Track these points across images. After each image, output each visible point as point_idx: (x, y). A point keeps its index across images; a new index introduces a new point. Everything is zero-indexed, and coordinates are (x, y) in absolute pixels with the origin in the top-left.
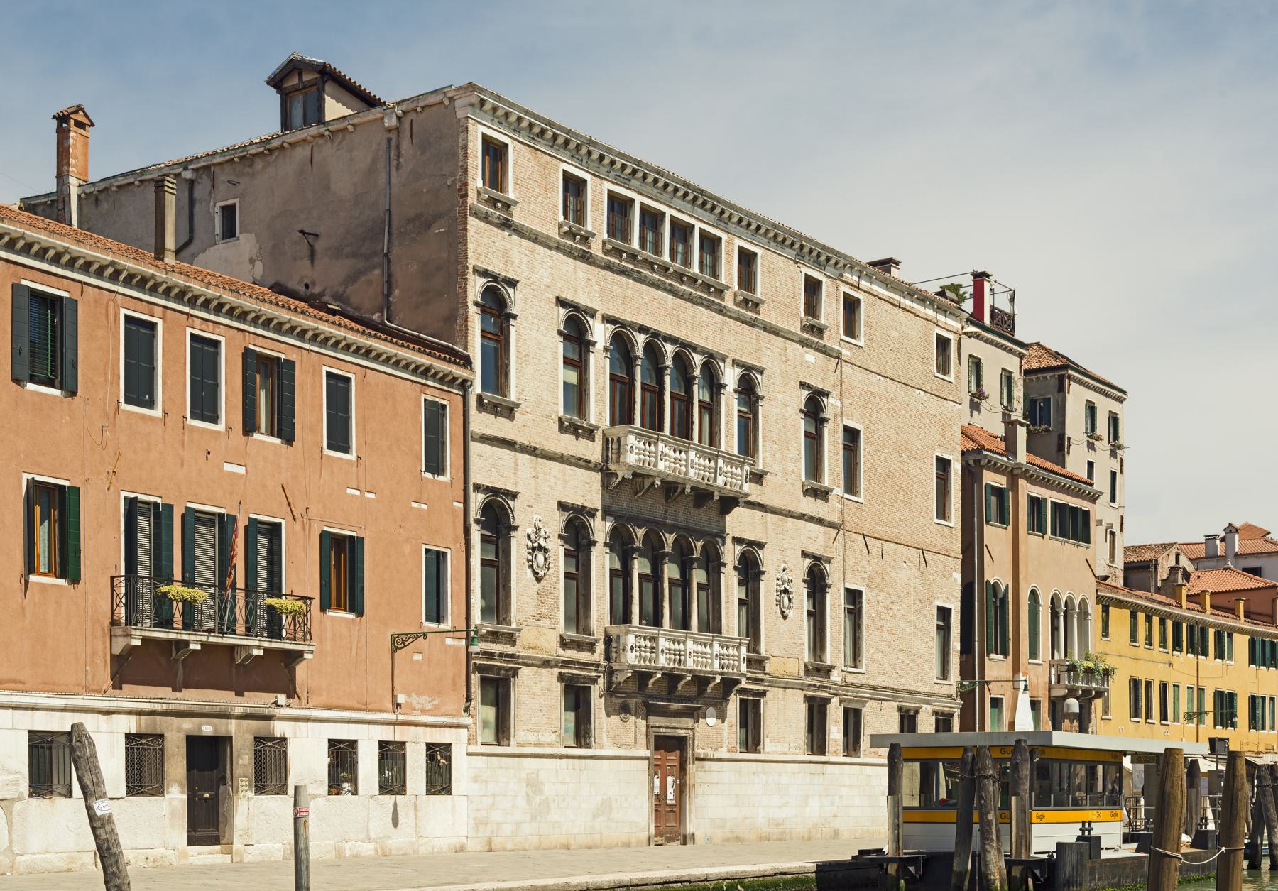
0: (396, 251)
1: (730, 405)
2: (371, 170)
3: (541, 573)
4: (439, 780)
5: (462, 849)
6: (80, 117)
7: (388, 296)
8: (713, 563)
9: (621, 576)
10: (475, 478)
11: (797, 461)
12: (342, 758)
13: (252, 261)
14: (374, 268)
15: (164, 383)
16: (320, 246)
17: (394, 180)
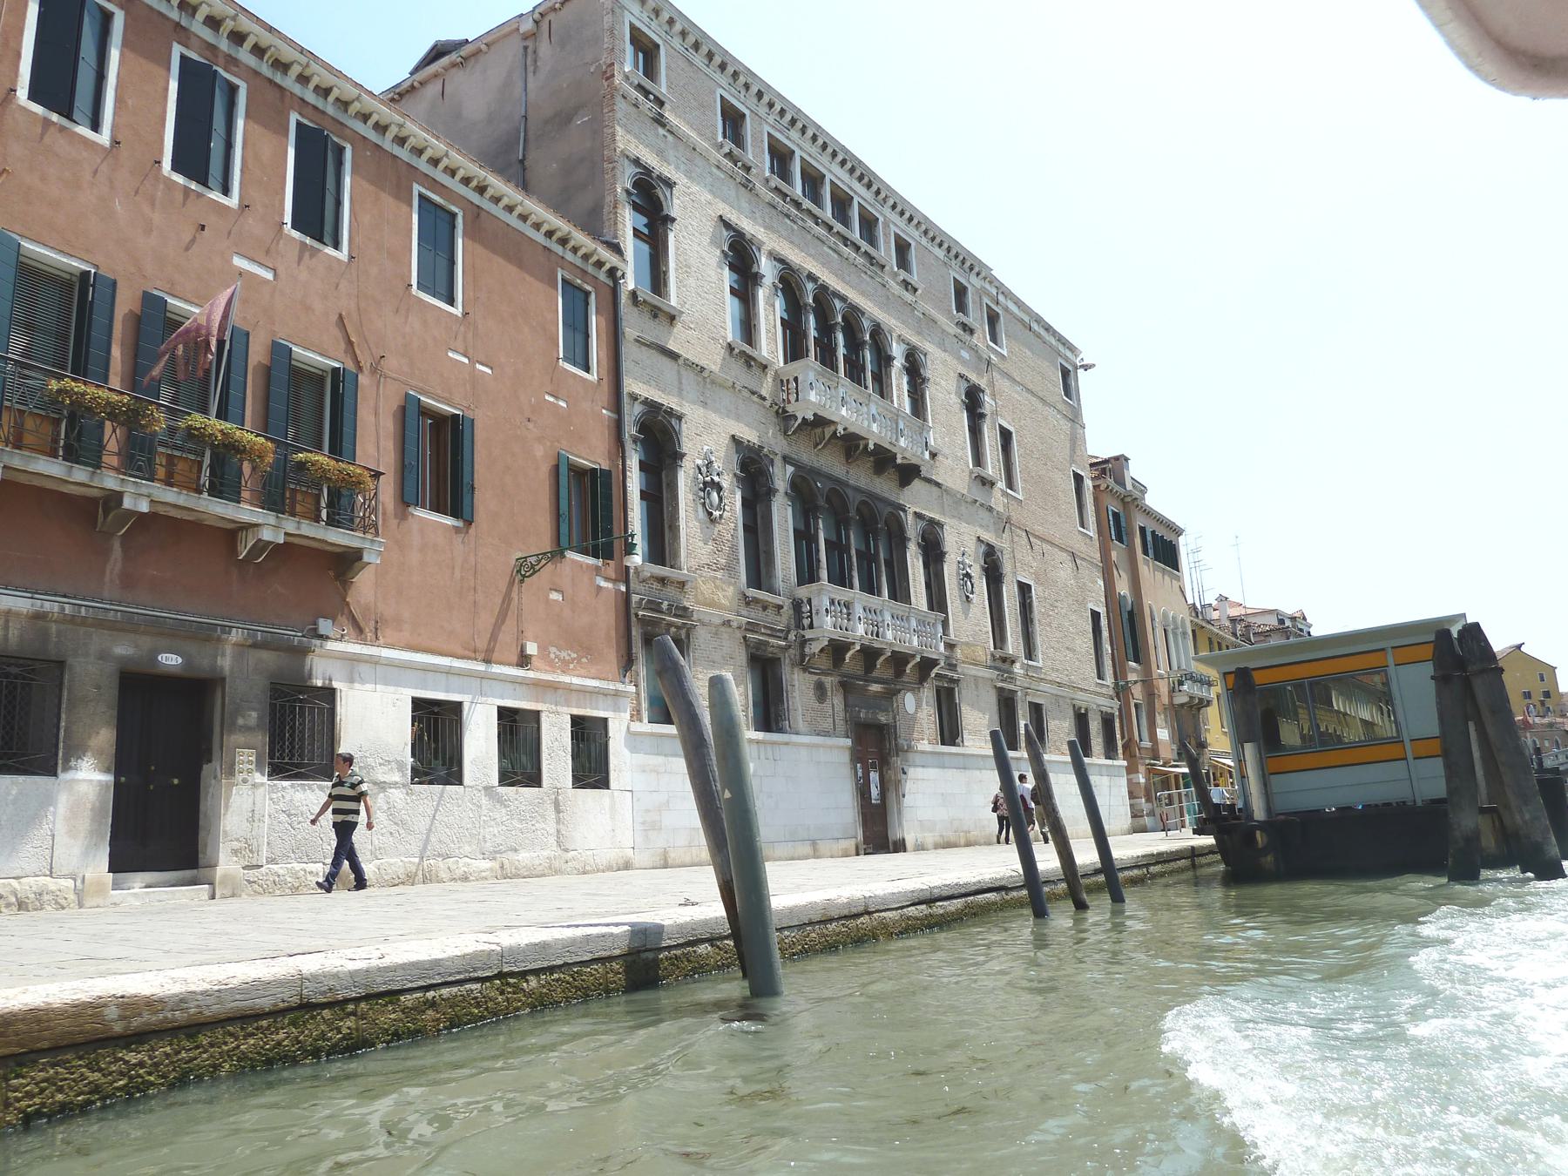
0: (531, 156)
3: (717, 513)
4: (591, 767)
8: (898, 540)
9: (804, 537)
10: (631, 385)
11: (963, 449)
12: (436, 730)
15: (119, 100)
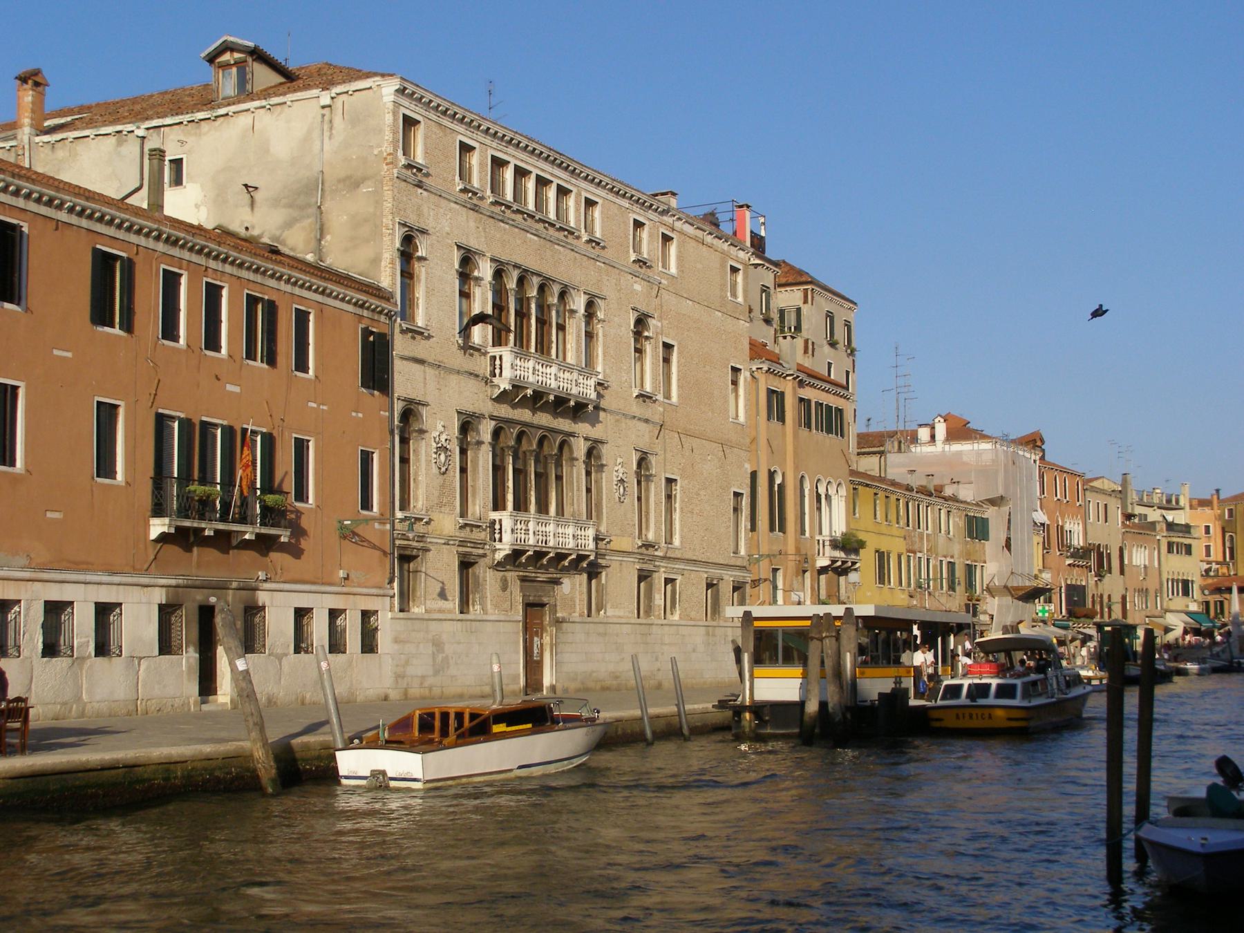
1: (575, 327)
2: (307, 139)
5: (386, 698)
6: (38, 79)
7: (320, 240)
13: (197, 206)
14: (308, 217)
16: (258, 196)
17: (326, 147)
